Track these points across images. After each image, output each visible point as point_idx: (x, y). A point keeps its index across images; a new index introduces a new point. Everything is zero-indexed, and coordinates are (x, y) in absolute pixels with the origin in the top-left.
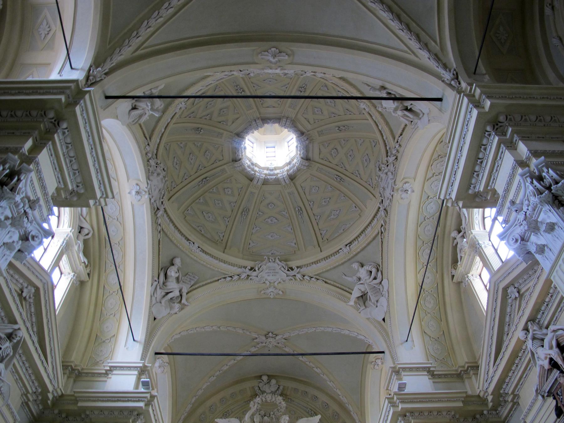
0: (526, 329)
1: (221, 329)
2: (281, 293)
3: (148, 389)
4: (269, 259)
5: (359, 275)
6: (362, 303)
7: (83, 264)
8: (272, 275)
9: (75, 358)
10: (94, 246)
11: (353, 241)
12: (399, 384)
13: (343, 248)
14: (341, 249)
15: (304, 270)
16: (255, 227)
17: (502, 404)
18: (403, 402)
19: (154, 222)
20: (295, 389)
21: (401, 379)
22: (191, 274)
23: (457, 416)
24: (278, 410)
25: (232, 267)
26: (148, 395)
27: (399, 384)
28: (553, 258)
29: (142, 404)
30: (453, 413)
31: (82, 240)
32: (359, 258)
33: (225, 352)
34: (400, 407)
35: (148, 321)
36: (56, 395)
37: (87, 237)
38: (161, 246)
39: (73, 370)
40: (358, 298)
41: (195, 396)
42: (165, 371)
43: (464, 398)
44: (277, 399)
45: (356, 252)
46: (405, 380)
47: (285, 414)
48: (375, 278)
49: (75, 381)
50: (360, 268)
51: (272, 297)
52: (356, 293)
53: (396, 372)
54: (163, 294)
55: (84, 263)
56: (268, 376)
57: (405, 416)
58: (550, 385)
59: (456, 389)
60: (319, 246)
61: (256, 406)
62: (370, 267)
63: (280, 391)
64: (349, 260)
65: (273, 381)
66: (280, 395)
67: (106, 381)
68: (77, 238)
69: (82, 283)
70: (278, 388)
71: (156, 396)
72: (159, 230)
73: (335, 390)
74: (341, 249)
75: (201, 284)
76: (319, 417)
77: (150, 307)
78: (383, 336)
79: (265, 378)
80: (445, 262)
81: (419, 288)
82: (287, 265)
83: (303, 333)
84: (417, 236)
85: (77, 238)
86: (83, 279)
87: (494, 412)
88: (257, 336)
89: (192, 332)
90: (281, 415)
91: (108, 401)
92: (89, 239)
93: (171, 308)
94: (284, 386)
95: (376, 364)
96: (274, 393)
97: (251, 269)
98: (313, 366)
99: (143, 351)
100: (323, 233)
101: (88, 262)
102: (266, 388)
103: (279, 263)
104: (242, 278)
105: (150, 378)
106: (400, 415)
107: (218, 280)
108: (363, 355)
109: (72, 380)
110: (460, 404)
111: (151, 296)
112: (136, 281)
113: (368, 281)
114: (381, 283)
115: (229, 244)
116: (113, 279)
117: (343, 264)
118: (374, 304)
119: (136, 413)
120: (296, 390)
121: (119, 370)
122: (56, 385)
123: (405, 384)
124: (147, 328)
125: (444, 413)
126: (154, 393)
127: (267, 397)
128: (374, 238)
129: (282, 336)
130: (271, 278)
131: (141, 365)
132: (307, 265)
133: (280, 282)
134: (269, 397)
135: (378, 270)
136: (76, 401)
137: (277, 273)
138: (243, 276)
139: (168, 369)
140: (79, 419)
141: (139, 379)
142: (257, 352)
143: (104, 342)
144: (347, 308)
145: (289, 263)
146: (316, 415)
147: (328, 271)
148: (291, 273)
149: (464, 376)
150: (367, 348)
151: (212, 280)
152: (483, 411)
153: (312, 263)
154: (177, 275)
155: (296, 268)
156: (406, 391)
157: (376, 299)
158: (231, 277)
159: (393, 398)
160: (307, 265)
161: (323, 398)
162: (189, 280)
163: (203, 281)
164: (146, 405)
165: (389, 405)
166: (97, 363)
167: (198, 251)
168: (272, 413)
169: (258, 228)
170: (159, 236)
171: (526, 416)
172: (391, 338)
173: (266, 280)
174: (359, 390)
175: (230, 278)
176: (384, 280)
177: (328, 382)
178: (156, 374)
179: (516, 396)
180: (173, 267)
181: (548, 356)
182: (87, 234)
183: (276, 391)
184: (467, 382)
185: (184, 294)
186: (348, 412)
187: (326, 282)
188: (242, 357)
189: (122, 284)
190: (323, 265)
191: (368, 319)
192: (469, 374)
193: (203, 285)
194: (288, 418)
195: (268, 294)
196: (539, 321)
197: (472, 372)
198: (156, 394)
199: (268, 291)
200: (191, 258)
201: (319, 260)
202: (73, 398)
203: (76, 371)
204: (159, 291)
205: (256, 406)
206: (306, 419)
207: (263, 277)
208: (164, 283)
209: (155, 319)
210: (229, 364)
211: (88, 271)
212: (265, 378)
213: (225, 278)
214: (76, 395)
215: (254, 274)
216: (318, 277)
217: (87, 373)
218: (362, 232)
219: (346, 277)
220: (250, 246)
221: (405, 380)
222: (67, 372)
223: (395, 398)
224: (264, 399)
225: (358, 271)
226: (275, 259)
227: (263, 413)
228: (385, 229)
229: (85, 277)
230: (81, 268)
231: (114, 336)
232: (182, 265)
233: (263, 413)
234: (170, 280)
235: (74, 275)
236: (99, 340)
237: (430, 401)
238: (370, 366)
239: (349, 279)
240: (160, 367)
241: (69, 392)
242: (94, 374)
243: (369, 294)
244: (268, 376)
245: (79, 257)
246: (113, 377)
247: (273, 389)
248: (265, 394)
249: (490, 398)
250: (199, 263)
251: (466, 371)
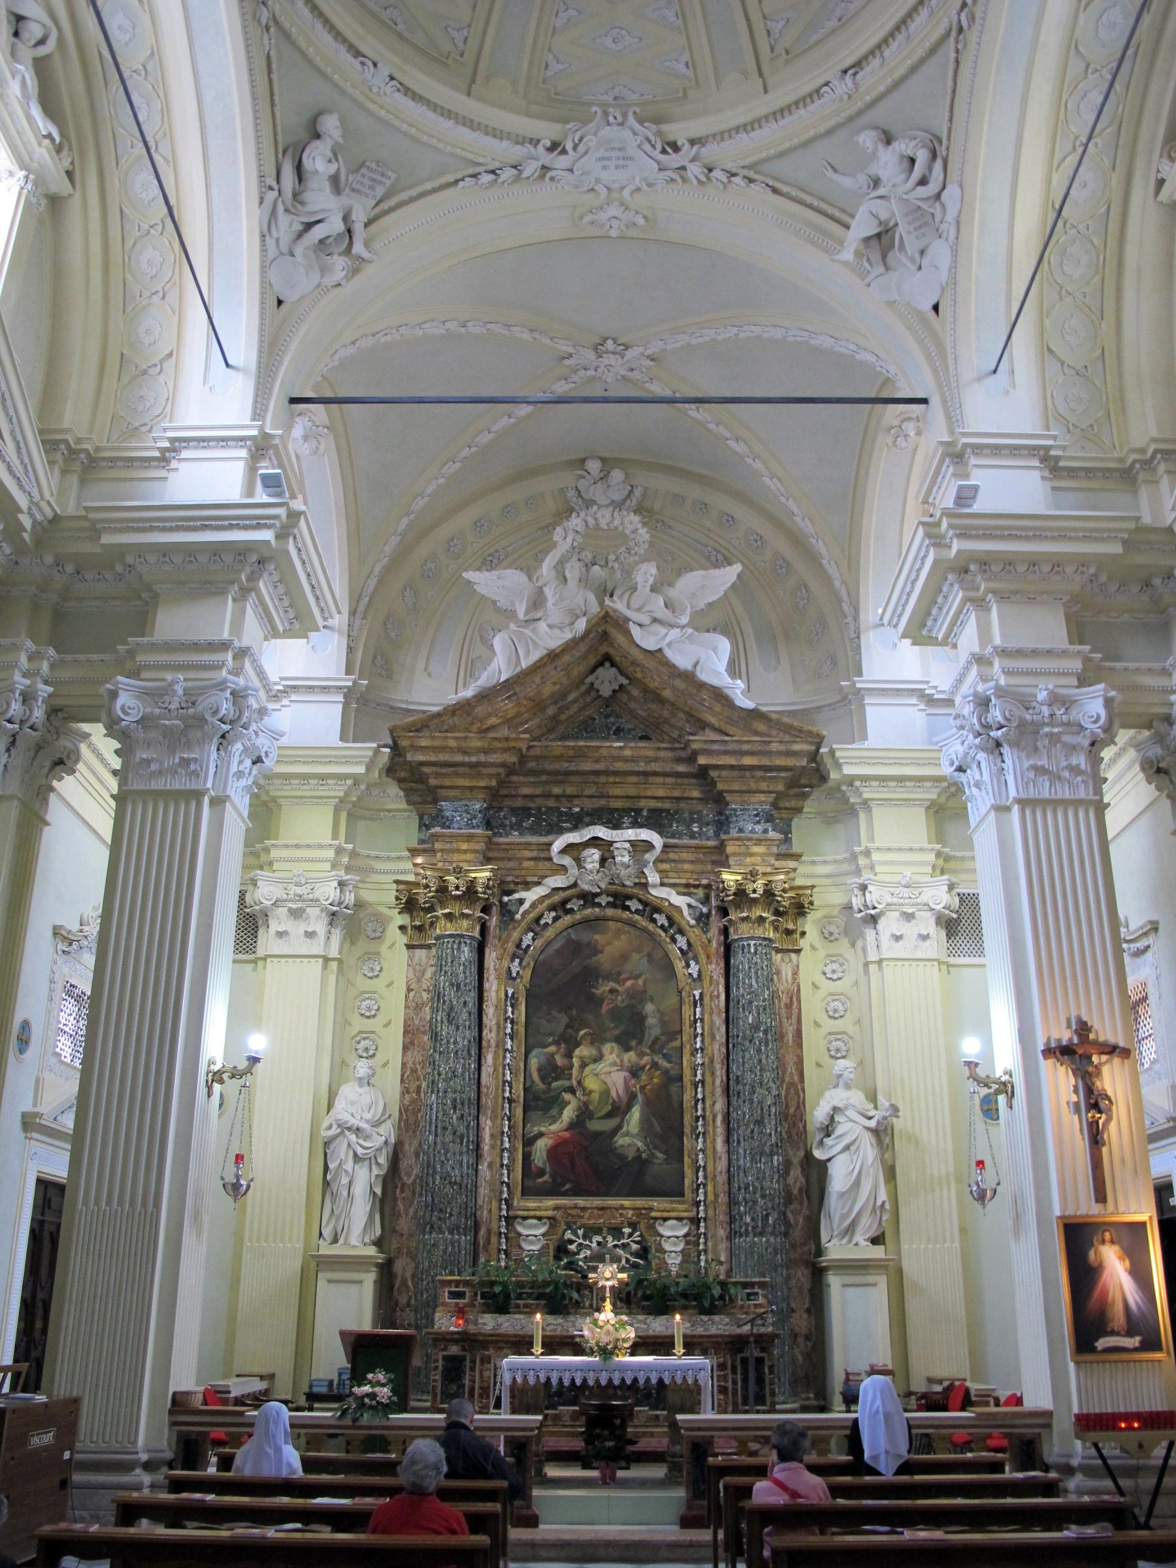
1: (471, 329)
2: (641, 221)
3: (280, 494)
4: (606, 114)
5: (874, 169)
6: (876, 257)
7: (47, 142)
8: (615, 166)
9: (74, 419)
10: (70, 80)
11: (865, 57)
12: (961, 488)
13: (835, 83)
14: (827, 84)
15: (710, 152)
16: (563, 8)
18: (964, 534)
19: (249, 16)
20: (676, 496)
21: (966, 476)
22: (373, 165)
23: (1103, 578)
24: (629, 550)
25: (496, 141)
26: (282, 511)
27: (961, 488)
29: (267, 535)
30: (1092, 570)
31: (30, 62)
32: (879, 115)
33: (485, 393)
34: (956, 546)
35: (262, 308)
36: (39, 517)
37: (42, 51)
38: (275, 76)
39: (73, 452)
40: (867, 240)
41: (408, 514)
42: (322, 447)
43: (1130, 532)
44: (626, 520)
45: (874, 94)
46: (977, 477)
47: (645, 559)
48: (923, 182)
49: (83, 482)
50: (881, 147)
51: (613, 233)
52: (862, 227)
53: (956, 456)
54: (300, 227)
55: (49, 136)
56: (603, 460)
57: (966, 571)
59: (1112, 508)
60: (761, 75)
61: (569, 539)
62: (913, 143)
63: (634, 502)
64: (851, 119)
65: (617, 475)
66: (635, 512)
67: (166, 479)
68: (13, 54)
69: (55, 202)
70: (631, 492)
71: (304, 513)
72: (264, 21)
73: (783, 499)
74: (827, 84)
75: (403, 196)
76: (737, 568)
77: (264, 269)
78: (928, 356)
79: (594, 466)
80: (1144, 136)
81: (1052, 216)
82: (659, 134)
83: (701, 340)
84: (1072, 46)
85: (13, 54)
86: (54, 189)
88: (571, 350)
89: (388, 338)
90: (637, 563)
91: (178, 529)
92: (47, 57)
93: (324, 270)
94: (646, 488)
95: (901, 433)
96: (618, 505)
97: (554, 147)
98: (727, 434)
99: (256, 396)
100: (776, 27)
101: (62, 134)
102: (597, 493)
103: (637, 127)
104: (524, 175)
105: (281, 465)
106: (952, 570)
107: (456, 182)
108: (869, 406)
109: (74, 479)
111: (263, 236)
112: (214, 191)
113: (901, 190)
114: (938, 196)
115: (482, 66)
116: (143, 185)
117: (829, 132)
118: (912, 260)
119: (254, 558)
120: (679, 499)
121: (196, 448)
122: (37, 497)
123: (976, 488)
124: (261, 330)
125: (1070, 570)
126: (297, 505)
127: (599, 515)
128: (933, 51)
129: (641, 349)
130: (611, 176)
131: (255, 432)
132: (721, 136)
133: (638, 189)
134: (605, 517)
135: (934, 155)
136: (94, 531)
137: (631, 158)
138: (530, 169)
139: (328, 443)
140: (109, 576)
141: (252, 469)
142: (572, 394)
143: (145, 372)
144: (831, 269)
145: (666, 128)
146: (730, 564)
147: (782, 155)
148: (673, 160)
149: (1141, 477)
150: (883, 385)
151: (436, 183)
153: (737, 129)
154: (333, 168)
155: (687, 145)
156: (977, 507)
157: (920, 245)
158: (493, 172)
159: (938, 524)
160: (721, 136)
161: (748, 519)
162: (367, 182)
163: (409, 188)
164: (277, 537)
165: (927, 542)
166: (134, 432)
167: (389, 89)
168: (612, 557)
169: (571, 12)
170: (266, 42)
172: (951, 362)
173: (598, 181)
174: (848, 501)
175: (491, 177)
176: (949, 188)
177: (767, 480)
178: (297, 457)
180: (318, 143)
182: (41, 42)
183: (624, 501)
184: (1144, 492)
185: (358, 228)
186: (812, 557)
187: (775, 191)
188: (530, 408)
189: (172, 202)
190: (769, 137)
191: (891, 304)
192: (1154, 470)
193: (412, 200)
194: (654, 571)
195: (602, 226)
198: (303, 508)
199: (603, 216)
200: (371, 113)
201: (759, 120)
202: (87, 524)
203: (82, 456)
204: (283, 219)
205: (569, 539)
206: (701, 572)
207: (588, 173)
208: (295, 195)
209: (280, 302)
210: (494, 429)
211: (66, 163)
212: (594, 466)
213: (475, 176)
214: (91, 516)
215: (562, 162)
216: (751, 174)
217: (111, 460)
218: (898, 28)
219: (836, 177)
220: (549, 73)
221: (977, 477)
222: (58, 457)
223: (944, 524)
224: (591, 521)
225: (874, 156)
226: (625, 115)
227: (590, 556)
228: (972, 19)
229: (61, 185)
230: (43, 153)
231: (171, 354)
232: (343, 136)
233: (588, 555)
234: (313, 183)
235: (27, 177)
236: (130, 368)
237: (1037, 535)
238: (884, 439)
239: (846, 182)
240: (306, 438)
241: (71, 510)
242: (130, 462)
243: (901, 229)
244: (603, 460)
245: (29, 118)
246: (183, 466)
247: (618, 496)
248: (595, 508)
250: (398, 130)
251: (1148, 464)
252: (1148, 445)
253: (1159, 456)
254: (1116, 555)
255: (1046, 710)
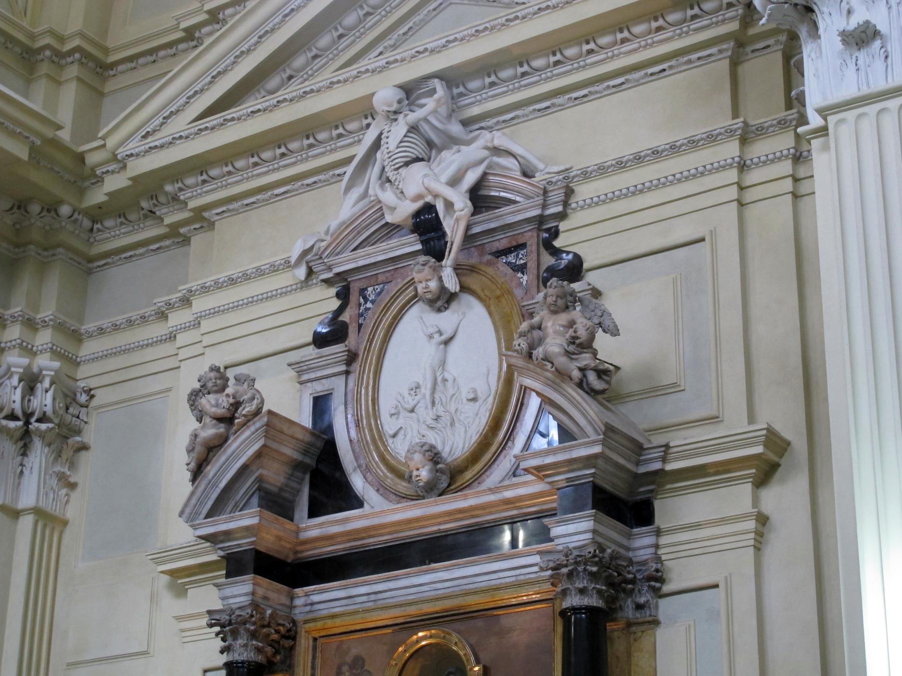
0: (410, 92)
17: (133, 217)
28: (880, 84)
58: (361, 263)
87: (87, 223)
110: (22, 152)
149: (45, 68)
152: (61, 202)
171: (205, 290)
179: (202, 219)
181: (429, 199)
192: (61, 67)
196: (461, 95)
197: (73, 71)
249: (115, 183)
251: (59, 57)
252: (72, 36)
253: (77, 56)
254: (19, 160)
255: (282, 651)
